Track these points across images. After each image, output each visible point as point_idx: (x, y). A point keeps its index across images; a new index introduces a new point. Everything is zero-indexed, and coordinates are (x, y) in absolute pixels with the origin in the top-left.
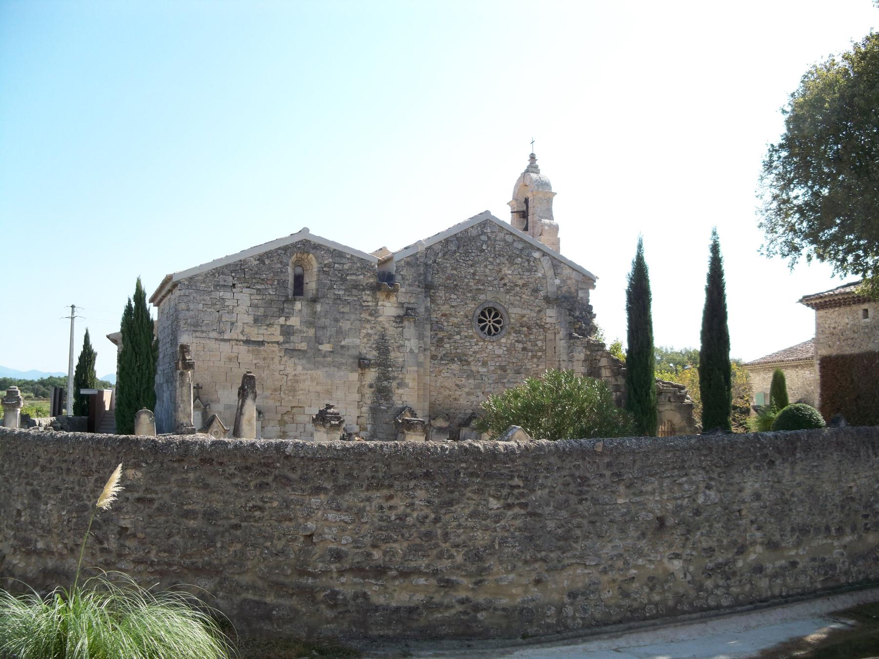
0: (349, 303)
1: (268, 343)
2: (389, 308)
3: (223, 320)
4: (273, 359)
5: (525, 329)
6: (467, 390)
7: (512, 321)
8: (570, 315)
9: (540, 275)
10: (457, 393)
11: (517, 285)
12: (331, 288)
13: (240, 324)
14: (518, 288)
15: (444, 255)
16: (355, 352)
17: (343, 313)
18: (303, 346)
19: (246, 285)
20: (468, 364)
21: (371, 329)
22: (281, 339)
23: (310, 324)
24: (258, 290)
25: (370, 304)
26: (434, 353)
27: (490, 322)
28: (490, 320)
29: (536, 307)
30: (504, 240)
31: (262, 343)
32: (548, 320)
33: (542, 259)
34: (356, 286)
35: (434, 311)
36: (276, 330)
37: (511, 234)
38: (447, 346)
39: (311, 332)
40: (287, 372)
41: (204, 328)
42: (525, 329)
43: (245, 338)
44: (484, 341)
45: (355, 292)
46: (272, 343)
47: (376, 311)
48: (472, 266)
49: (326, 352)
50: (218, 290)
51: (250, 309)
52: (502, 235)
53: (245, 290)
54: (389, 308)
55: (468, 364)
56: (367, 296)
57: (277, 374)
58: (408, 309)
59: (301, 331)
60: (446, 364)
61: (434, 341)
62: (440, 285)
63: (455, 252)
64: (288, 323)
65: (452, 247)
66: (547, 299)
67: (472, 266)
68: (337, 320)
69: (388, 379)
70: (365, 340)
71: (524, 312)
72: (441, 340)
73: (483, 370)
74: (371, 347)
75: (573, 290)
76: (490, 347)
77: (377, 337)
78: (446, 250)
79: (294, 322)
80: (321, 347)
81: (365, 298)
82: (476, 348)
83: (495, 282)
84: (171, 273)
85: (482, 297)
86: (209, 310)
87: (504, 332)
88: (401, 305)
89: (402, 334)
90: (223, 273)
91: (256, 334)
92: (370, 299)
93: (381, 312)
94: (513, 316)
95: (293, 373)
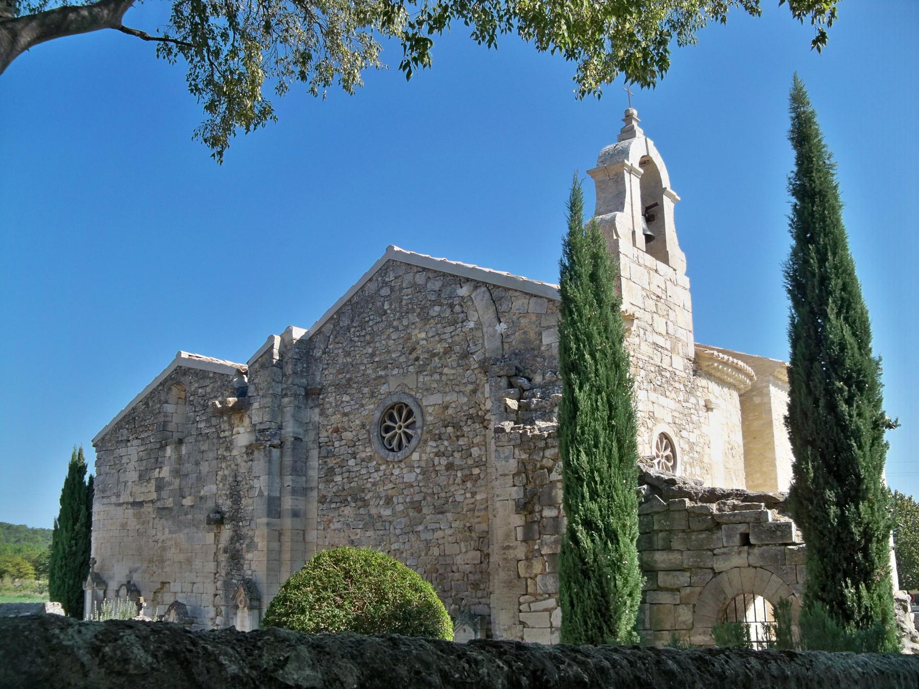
7: (429, 419)
11: (434, 355)
24: (143, 439)
37: (424, 269)
40: (157, 537)
43: (131, 500)
47: (231, 442)
48: (369, 343)
52: (409, 278)
61: (322, 474)
63: (348, 330)
68: (197, 463)
72: (332, 469)
73: (387, 512)
85: (384, 389)
94: (430, 410)
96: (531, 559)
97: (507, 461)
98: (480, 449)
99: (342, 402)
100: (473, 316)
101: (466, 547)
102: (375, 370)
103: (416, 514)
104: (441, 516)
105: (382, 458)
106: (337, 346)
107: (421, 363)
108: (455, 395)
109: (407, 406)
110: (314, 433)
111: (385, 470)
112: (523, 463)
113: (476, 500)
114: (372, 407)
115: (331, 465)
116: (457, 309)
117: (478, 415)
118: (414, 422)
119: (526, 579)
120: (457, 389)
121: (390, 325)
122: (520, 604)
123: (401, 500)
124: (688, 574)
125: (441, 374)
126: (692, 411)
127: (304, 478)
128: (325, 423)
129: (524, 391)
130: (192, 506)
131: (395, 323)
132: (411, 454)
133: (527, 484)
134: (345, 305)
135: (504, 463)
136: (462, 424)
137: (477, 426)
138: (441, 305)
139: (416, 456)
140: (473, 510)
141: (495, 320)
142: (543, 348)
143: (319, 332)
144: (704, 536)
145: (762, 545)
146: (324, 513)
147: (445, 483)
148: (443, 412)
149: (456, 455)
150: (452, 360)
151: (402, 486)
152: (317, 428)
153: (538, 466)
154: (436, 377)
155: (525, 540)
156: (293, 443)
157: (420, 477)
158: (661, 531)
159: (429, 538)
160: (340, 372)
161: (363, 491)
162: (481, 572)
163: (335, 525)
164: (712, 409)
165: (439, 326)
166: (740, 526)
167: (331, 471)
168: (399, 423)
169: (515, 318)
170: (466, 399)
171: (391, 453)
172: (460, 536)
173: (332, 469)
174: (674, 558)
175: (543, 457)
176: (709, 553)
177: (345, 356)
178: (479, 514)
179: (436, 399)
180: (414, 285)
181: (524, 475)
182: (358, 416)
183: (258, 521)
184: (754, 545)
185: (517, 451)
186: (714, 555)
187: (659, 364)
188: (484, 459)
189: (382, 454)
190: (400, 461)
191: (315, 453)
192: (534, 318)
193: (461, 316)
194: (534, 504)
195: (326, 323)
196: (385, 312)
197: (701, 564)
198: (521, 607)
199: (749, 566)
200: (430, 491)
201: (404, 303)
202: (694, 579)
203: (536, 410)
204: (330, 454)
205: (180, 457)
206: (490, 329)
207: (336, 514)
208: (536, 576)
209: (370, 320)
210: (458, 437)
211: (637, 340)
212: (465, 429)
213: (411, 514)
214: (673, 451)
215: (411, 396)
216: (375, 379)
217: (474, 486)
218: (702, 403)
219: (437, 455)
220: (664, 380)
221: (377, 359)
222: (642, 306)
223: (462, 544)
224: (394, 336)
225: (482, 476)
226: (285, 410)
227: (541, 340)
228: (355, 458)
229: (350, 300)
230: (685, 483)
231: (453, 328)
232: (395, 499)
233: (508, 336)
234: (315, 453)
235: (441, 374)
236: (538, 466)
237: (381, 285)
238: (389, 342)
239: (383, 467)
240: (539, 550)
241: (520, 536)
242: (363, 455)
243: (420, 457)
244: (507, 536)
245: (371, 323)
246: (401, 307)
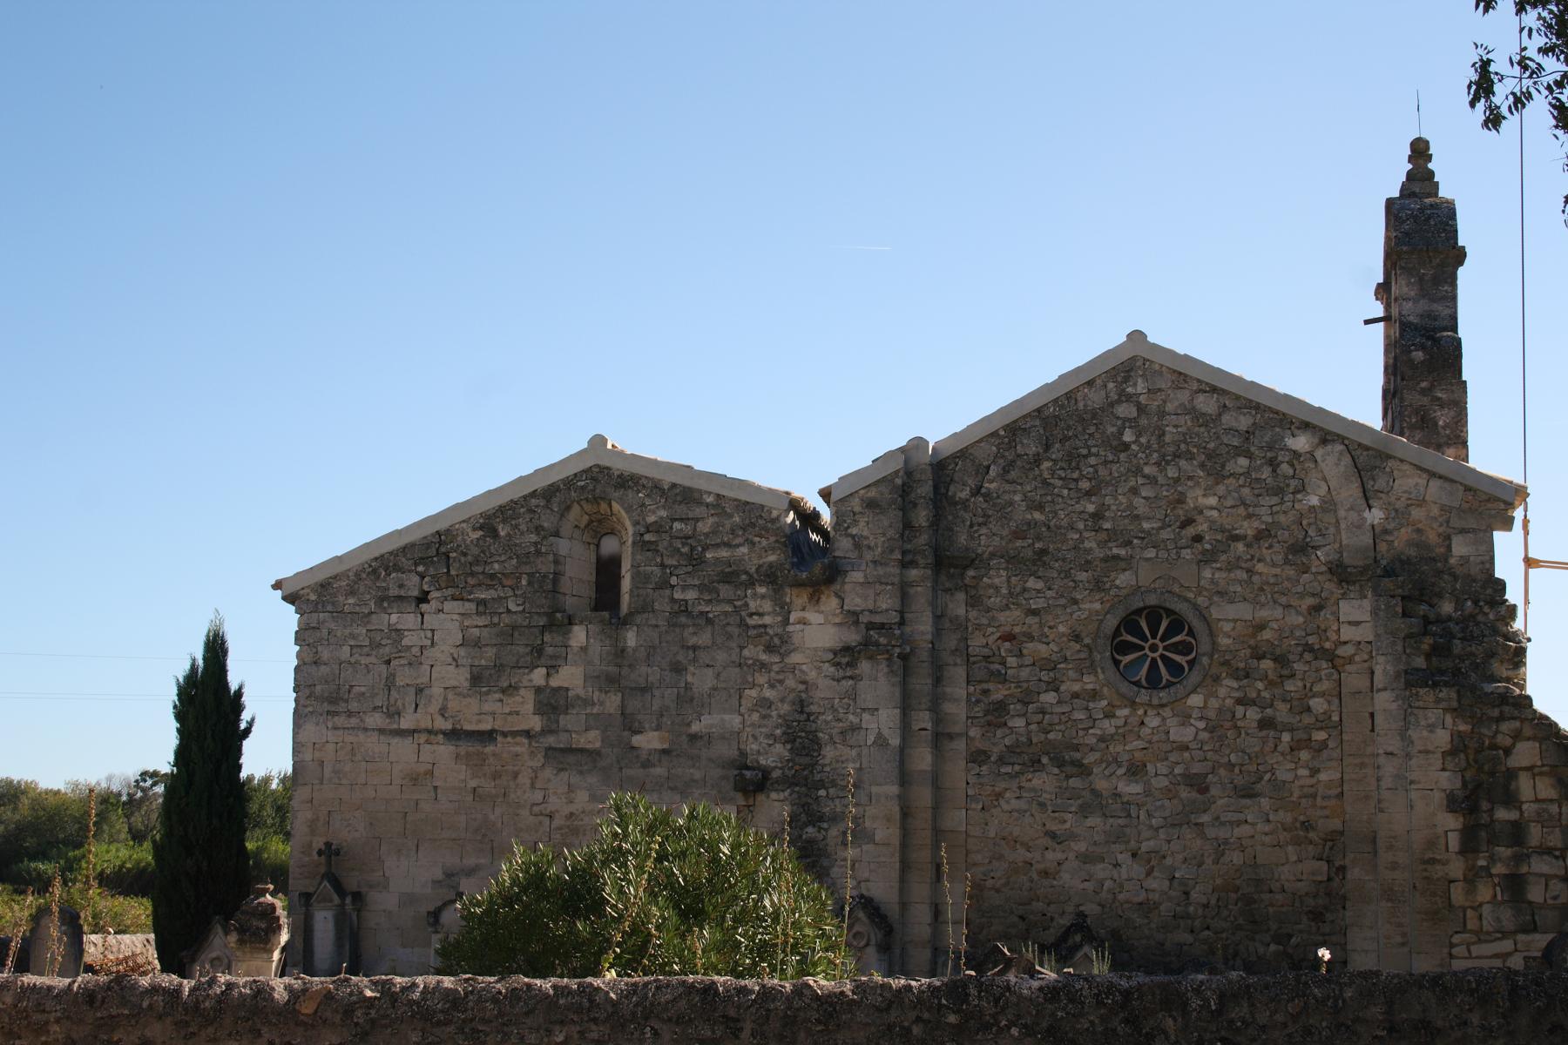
0: (709, 621)
1: (505, 734)
2: (817, 628)
3: (400, 682)
4: (516, 775)
5: (1267, 664)
6: (1082, 847)
7: (1224, 641)
8: (1405, 614)
9: (1314, 501)
10: (1050, 855)
11: (1236, 538)
12: (664, 584)
13: (436, 690)
14: (1240, 547)
15: (1006, 471)
16: (728, 751)
17: (695, 648)
18: (592, 740)
19: (450, 591)
21: (772, 686)
22: (536, 723)
23: (611, 682)
24: (480, 602)
25: (767, 620)
26: (979, 745)
27: (1155, 649)
28: (1152, 641)
29: (1302, 596)
30: (1192, 411)
31: (489, 736)
32: (1347, 633)
33: (1319, 454)
34: (730, 575)
35: (978, 627)
36: (525, 702)
38: (1019, 723)
39: (613, 702)
40: (550, 808)
41: (354, 706)
42: (1267, 664)
43: (448, 726)
44: (1133, 704)
45: (725, 591)
46: (515, 734)
47: (785, 639)
49: (650, 752)
50: (385, 610)
51: (462, 651)
52: (1183, 397)
53: (448, 606)
54: (817, 628)
55: (1084, 771)
56: (760, 601)
57: (525, 812)
58: (870, 626)
59: (587, 702)
60: (1017, 775)
61: (978, 710)
62: (993, 555)
63: (1037, 461)
64: (554, 683)
65: (1030, 447)
66: (1341, 573)
67: (1089, 494)
68: (678, 669)
69: (816, 819)
70: (755, 716)
71: (1264, 613)
72: (1001, 708)
73: (1132, 789)
74: (770, 736)
75: (1432, 537)
76: (1153, 722)
77: (786, 708)
78: (1010, 455)
79: (570, 677)
80: (637, 740)
81: (753, 605)
82: (1108, 726)
83: (1165, 534)
84: (280, 577)
85: (1124, 579)
86: (364, 660)
87: (1194, 677)
88: (853, 617)
89: (853, 695)
90: (398, 568)
91: (476, 713)
92: (767, 606)
93: (796, 640)
94: (1227, 627)
95: (567, 810)
99: (1025, 590)
102: (1102, 544)
103: (1194, 795)
104: (1248, 801)
111: (1126, 717)
112: (1457, 736)
116: (1285, 469)
119: (1464, 910)
120: (1283, 600)
121: (1138, 471)
122: (1452, 946)
130: (664, 751)
135: (1425, 733)
142: (1452, 561)
147: (1257, 749)
148: (1254, 635)
155: (1462, 852)
157: (1204, 735)
161: (1076, 748)
162: (1328, 894)
163: (1011, 802)
168: (1157, 641)
170: (1301, 619)
175: (1497, 732)
177: (1029, 508)
183: (874, 789)
188: (1335, 718)
190: (1162, 706)
193: (1293, 483)
195: (981, 441)
198: (1455, 951)
205: (620, 652)
208: (1481, 905)
215: (1187, 600)
217: (1313, 758)
219: (1239, 702)
221: (1107, 525)
225: (1331, 744)
226: (912, 591)
227: (1449, 548)
228: (1057, 690)
229: (1039, 410)
231: (1275, 500)
232: (1149, 767)
233: (1386, 532)
234: (960, 673)
235: (1248, 571)
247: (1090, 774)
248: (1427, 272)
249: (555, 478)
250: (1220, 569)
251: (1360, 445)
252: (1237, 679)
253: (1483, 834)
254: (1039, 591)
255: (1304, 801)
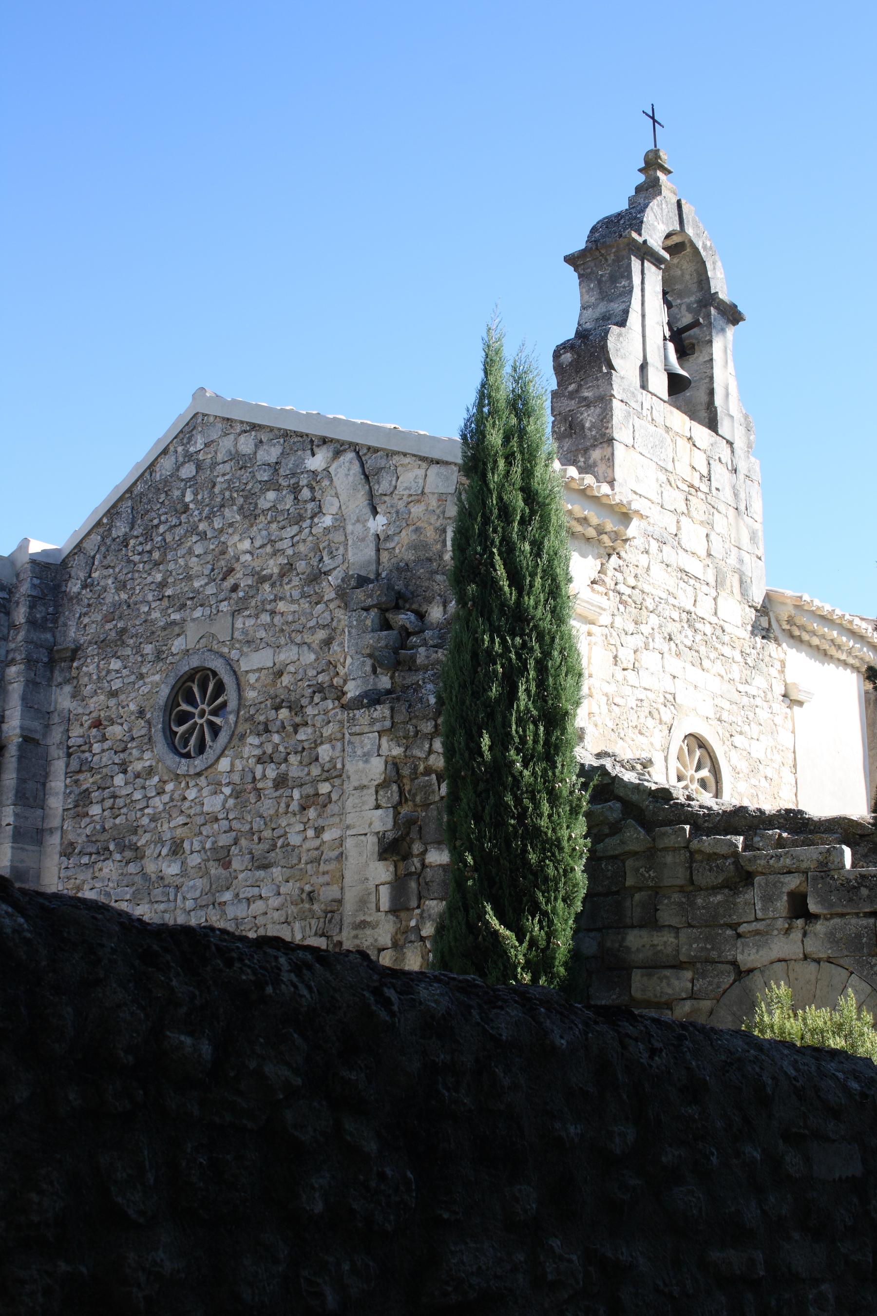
5: (284, 713)
7: (251, 695)
11: (263, 579)
20: (138, 854)
28: (194, 705)
37: (254, 427)
42: (284, 713)
48: (157, 564)
52: (227, 443)
65: (121, 529)
71: (282, 657)
72: (86, 794)
73: (172, 869)
85: (178, 645)
94: (252, 678)
96: (403, 947)
97: (367, 761)
98: (333, 747)
99: (108, 672)
100: (331, 506)
101: (303, 929)
104: (261, 873)
105: (169, 770)
106: (106, 572)
107: (241, 594)
108: (295, 649)
109: (215, 674)
110: (61, 729)
112: (394, 766)
113: (323, 842)
114: (157, 678)
115: (84, 787)
116: (306, 493)
117: (332, 685)
118: (224, 704)
121: (194, 530)
123: (197, 846)
124: (689, 975)
125: (273, 613)
126: (758, 701)
127: (39, 812)
128: (80, 711)
129: (409, 635)
131: (202, 526)
132: (218, 758)
133: (400, 803)
134: (121, 499)
135: (361, 765)
136: (304, 702)
137: (329, 704)
138: (278, 489)
139: (224, 764)
140: (317, 861)
141: (367, 511)
143: (78, 548)
144: (719, 898)
145: (833, 916)
146: (70, 873)
147: (272, 812)
148: (274, 683)
149: (293, 759)
150: (292, 587)
151: (200, 820)
152: (68, 720)
153: (421, 768)
154: (265, 618)
155: (394, 910)
156: (20, 747)
157: (231, 802)
158: (640, 889)
159: (240, 915)
160: (108, 618)
164: (800, 703)
165: (274, 526)
166: (787, 879)
167: (84, 798)
168: (201, 706)
169: (401, 505)
170: (313, 657)
171: (183, 761)
172: (293, 910)
173: (86, 794)
174: (665, 941)
175: (430, 752)
176: (729, 932)
177: (117, 589)
178: (326, 869)
179: (262, 659)
180: (235, 456)
181: (395, 787)
182: (133, 695)
184: (816, 917)
185: (384, 740)
186: (739, 936)
187: (689, 607)
189: (169, 762)
190: (199, 774)
191: (59, 766)
192: (434, 503)
193: (310, 506)
194: (412, 841)
195: (89, 534)
196: (186, 509)
197: (714, 954)
199: (805, 957)
200: (248, 827)
201: (217, 490)
202: (699, 984)
203: (425, 668)
204: (85, 767)
206: (359, 526)
207: (90, 876)
209: (161, 523)
210: (296, 727)
211: (643, 560)
212: (310, 711)
213: (213, 871)
214: (716, 771)
215: (222, 655)
216: (164, 629)
217: (319, 816)
218: (779, 690)
219: (260, 760)
220: (699, 637)
222: (656, 498)
223: (297, 926)
224: (198, 550)
225: (334, 797)
228: (125, 772)
229: (130, 490)
230: (689, 798)
231: (295, 529)
232: (186, 845)
233: (388, 538)
235: (273, 613)
236: (421, 768)
237: (181, 459)
238: (193, 559)
239: (169, 787)
240: (417, 929)
241: (385, 904)
242: (138, 766)
243: (232, 765)
244: (362, 902)
245: (161, 529)
246: (212, 496)
247: (142, 858)
248: (604, 272)
249: (868, 779)
250: (249, 616)
251: (369, 448)
252: (259, 735)
253: (413, 885)
254: (117, 671)
255: (309, 866)
